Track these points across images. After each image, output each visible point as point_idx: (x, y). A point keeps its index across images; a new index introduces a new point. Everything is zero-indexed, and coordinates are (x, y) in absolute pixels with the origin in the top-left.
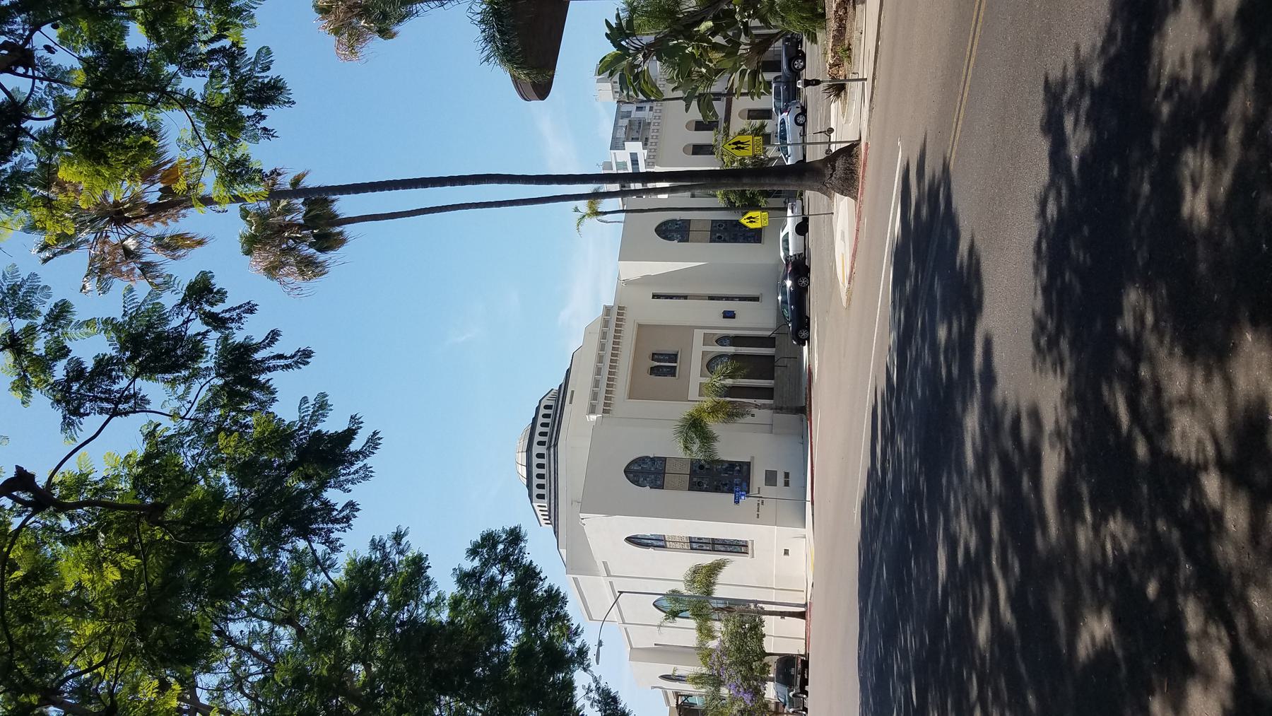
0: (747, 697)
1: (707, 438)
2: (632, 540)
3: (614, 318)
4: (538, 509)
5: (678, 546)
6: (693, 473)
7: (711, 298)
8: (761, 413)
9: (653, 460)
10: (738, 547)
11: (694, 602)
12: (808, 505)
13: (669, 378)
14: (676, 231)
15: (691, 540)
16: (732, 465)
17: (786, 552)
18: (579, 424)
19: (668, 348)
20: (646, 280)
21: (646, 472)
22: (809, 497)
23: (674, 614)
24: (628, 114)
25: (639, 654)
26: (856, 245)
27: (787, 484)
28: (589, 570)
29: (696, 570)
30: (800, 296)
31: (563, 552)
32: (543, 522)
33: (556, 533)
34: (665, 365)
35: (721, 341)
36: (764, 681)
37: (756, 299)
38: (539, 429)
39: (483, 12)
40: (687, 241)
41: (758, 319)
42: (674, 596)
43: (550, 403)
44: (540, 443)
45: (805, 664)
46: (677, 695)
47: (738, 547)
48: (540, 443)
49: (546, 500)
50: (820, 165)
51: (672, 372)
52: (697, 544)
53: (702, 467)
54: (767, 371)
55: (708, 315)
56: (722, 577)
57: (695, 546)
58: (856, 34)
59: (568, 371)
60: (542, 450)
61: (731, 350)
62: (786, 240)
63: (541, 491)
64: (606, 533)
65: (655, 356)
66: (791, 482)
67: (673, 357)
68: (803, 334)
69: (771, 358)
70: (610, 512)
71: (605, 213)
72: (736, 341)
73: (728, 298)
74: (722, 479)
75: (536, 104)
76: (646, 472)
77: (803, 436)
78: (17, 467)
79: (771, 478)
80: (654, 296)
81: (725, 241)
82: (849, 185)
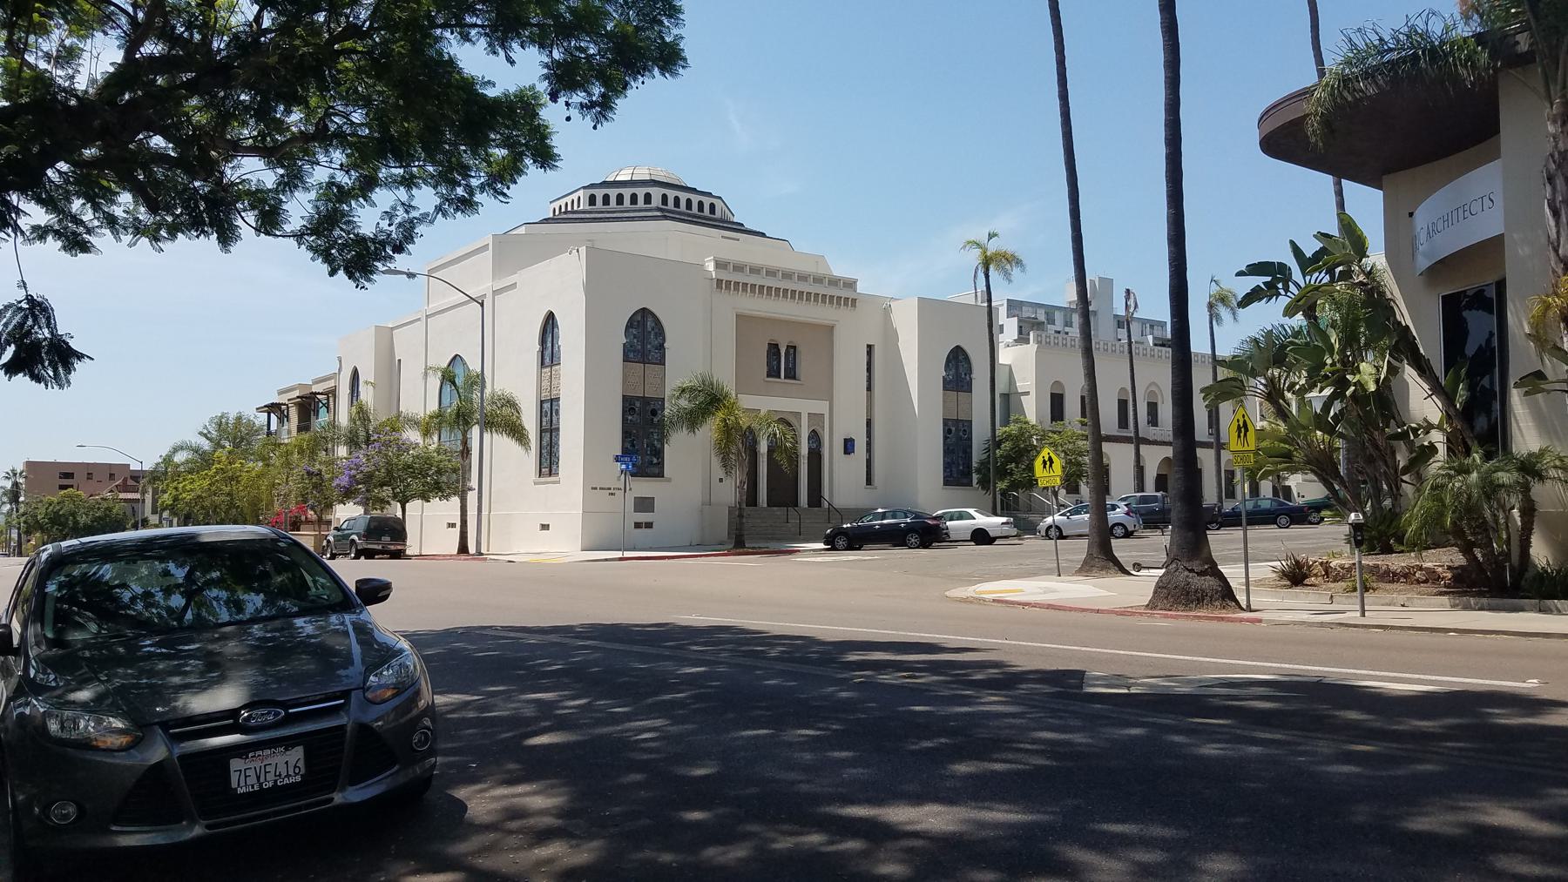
0: (344, 481)
1: (693, 419)
2: (550, 321)
3: (842, 294)
4: (575, 197)
5: (546, 384)
6: (645, 401)
7: (869, 423)
8: (728, 491)
9: (661, 347)
10: (548, 462)
11: (469, 408)
12: (619, 554)
13: (765, 369)
14: (957, 374)
15: (554, 401)
16: (659, 453)
17: (545, 527)
18: (703, 250)
19: (803, 368)
20: (891, 335)
21: (644, 338)
22: (628, 554)
23: (448, 378)
24: (1051, 321)
25: (385, 339)
26: (1071, 609)
27: (638, 525)
28: (499, 268)
29: (511, 403)
30: (894, 537)
31: (522, 230)
32: (556, 205)
33: (546, 221)
34: (781, 362)
35: (815, 437)
36: (364, 503)
37: (869, 481)
38: (683, 196)
39: (1425, 35)
40: (945, 388)
41: (844, 483)
42: (478, 381)
43: (718, 214)
44: (665, 198)
45: (398, 555)
46: (332, 393)
47: (548, 462)
48: (665, 198)
49: (588, 208)
50: (1204, 555)
51: (773, 372)
52: (549, 408)
53: (654, 413)
54: (777, 499)
55: (847, 421)
56: (500, 443)
57: (547, 406)
58: (1402, 598)
59: (763, 235)
60: (656, 201)
61: (804, 450)
62: (961, 517)
63: (599, 201)
64: (561, 283)
65: (792, 349)
66: (640, 531)
67: (791, 374)
68: (841, 542)
69: (795, 503)
70: (590, 288)
71: (987, 277)
72: (815, 456)
73: (869, 444)
74: (642, 437)
75: (1255, 137)
76: (644, 338)
77: (703, 545)
78: (228, 251)
79: (644, 504)
80: (870, 347)
81: (945, 438)
82: (1172, 595)
